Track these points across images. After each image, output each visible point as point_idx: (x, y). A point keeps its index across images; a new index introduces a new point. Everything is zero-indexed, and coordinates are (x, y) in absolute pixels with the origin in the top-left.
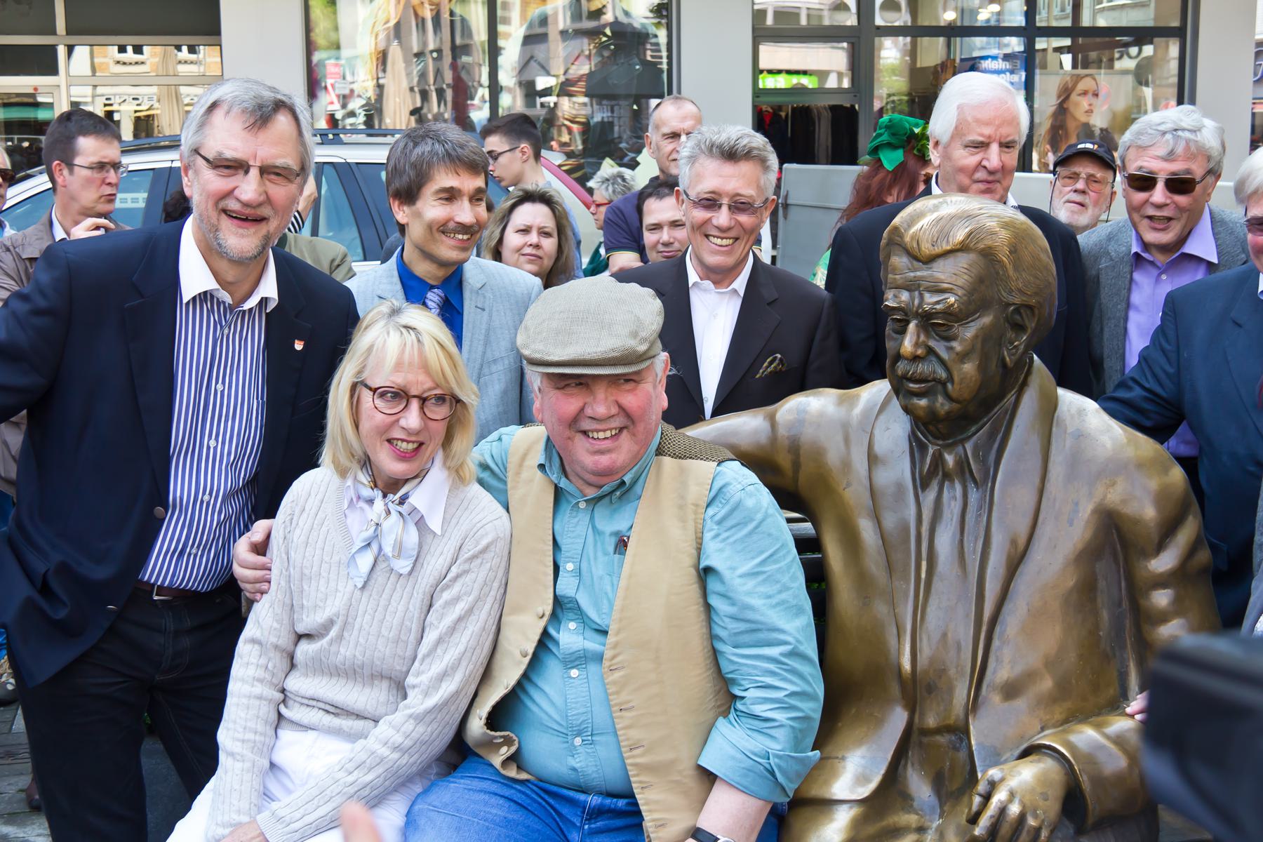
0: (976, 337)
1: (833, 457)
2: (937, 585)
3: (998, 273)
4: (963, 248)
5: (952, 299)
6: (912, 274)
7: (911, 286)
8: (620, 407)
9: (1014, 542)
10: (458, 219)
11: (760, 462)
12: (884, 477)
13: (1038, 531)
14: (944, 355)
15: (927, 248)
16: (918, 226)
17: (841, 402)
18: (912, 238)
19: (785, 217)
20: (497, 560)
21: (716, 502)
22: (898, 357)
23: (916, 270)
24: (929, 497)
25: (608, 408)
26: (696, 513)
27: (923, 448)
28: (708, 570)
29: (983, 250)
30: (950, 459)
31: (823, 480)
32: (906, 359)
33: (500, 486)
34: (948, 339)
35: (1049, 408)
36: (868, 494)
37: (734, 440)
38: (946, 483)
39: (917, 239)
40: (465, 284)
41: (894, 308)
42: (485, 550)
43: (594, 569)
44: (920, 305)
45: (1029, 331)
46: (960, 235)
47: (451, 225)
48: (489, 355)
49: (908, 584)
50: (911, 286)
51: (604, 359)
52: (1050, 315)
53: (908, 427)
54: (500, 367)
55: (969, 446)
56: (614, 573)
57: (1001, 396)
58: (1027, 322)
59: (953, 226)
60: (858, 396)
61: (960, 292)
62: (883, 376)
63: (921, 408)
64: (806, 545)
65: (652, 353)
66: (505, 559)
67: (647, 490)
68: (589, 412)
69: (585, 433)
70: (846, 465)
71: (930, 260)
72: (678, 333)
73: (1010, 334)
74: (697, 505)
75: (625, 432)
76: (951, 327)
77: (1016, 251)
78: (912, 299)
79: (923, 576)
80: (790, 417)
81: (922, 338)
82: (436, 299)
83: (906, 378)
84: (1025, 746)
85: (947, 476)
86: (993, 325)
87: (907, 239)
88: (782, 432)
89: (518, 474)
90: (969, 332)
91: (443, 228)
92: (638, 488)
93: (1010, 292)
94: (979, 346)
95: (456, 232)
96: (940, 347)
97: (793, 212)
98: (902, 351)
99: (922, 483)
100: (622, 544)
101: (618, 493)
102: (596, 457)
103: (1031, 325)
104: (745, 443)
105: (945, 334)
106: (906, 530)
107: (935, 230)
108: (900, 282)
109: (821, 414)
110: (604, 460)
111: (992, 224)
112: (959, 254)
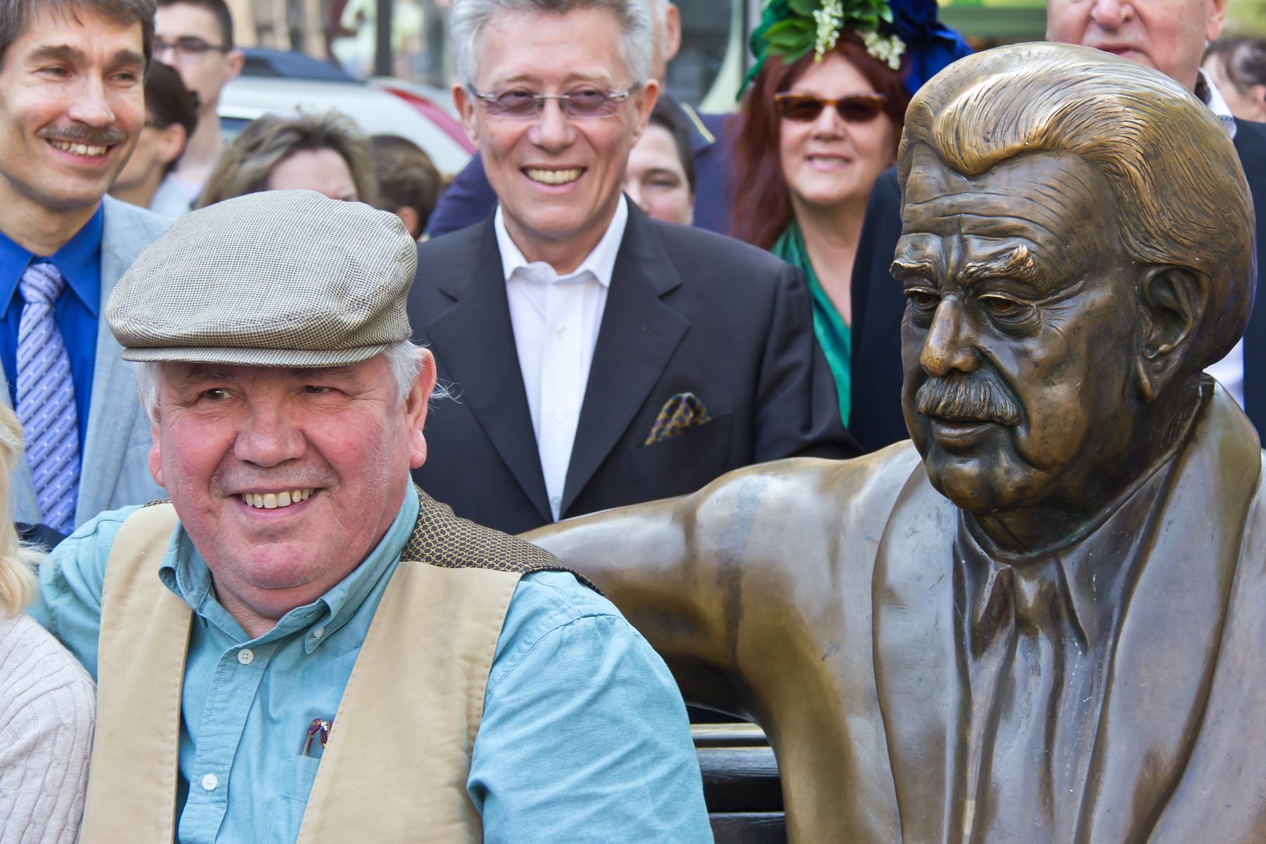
0: (1075, 330)
1: (807, 593)
3: (1119, 199)
4: (1047, 146)
5: (1022, 250)
6: (947, 201)
7: (945, 226)
8: (310, 443)
9: (1151, 759)
10: (77, 113)
11: (655, 608)
12: (896, 630)
13: (1206, 738)
14: (1011, 367)
15: (975, 147)
17: (825, 485)
18: (947, 126)
20: (56, 773)
21: (514, 653)
22: (922, 375)
24: (986, 671)
25: (283, 442)
26: (470, 676)
27: (978, 567)
28: (481, 792)
29: (1089, 150)
30: (1029, 590)
31: (787, 642)
32: (934, 375)
33: (87, 622)
37: (609, 561)
38: (1022, 639)
40: (106, 257)
41: (911, 272)
42: (28, 751)
43: (255, 786)
46: (1040, 119)
47: (63, 125)
50: (945, 226)
51: (269, 335)
52: (1239, 293)
55: (1070, 565)
56: (296, 794)
57: (1138, 462)
58: (1186, 306)
59: (1027, 102)
60: (862, 472)
61: (1040, 236)
65: (380, 333)
66: (76, 769)
67: (376, 632)
68: (242, 450)
69: (239, 497)
70: (834, 610)
71: (983, 170)
72: (465, 320)
73: (1151, 330)
74: (473, 660)
75: (322, 498)
76: (1023, 309)
77: (1157, 155)
78: (946, 250)
79: (968, 829)
80: (725, 513)
81: (966, 331)
82: (43, 283)
84: (195, 541)
85: (1024, 624)
86: (1109, 310)
87: (937, 128)
88: (707, 543)
89: (122, 596)
90: (1061, 319)
91: (48, 130)
92: (358, 623)
93: (1147, 238)
94: (1082, 348)
95: (73, 139)
96: (1002, 351)
99: (974, 639)
100: (316, 737)
101: (318, 632)
102: (261, 547)
103: (1195, 310)
104: (627, 563)
105: (1011, 323)
106: (937, 739)
107: (991, 109)
108: (923, 218)
109: (787, 507)
110: (276, 554)
111: (1109, 97)
112: (1040, 158)
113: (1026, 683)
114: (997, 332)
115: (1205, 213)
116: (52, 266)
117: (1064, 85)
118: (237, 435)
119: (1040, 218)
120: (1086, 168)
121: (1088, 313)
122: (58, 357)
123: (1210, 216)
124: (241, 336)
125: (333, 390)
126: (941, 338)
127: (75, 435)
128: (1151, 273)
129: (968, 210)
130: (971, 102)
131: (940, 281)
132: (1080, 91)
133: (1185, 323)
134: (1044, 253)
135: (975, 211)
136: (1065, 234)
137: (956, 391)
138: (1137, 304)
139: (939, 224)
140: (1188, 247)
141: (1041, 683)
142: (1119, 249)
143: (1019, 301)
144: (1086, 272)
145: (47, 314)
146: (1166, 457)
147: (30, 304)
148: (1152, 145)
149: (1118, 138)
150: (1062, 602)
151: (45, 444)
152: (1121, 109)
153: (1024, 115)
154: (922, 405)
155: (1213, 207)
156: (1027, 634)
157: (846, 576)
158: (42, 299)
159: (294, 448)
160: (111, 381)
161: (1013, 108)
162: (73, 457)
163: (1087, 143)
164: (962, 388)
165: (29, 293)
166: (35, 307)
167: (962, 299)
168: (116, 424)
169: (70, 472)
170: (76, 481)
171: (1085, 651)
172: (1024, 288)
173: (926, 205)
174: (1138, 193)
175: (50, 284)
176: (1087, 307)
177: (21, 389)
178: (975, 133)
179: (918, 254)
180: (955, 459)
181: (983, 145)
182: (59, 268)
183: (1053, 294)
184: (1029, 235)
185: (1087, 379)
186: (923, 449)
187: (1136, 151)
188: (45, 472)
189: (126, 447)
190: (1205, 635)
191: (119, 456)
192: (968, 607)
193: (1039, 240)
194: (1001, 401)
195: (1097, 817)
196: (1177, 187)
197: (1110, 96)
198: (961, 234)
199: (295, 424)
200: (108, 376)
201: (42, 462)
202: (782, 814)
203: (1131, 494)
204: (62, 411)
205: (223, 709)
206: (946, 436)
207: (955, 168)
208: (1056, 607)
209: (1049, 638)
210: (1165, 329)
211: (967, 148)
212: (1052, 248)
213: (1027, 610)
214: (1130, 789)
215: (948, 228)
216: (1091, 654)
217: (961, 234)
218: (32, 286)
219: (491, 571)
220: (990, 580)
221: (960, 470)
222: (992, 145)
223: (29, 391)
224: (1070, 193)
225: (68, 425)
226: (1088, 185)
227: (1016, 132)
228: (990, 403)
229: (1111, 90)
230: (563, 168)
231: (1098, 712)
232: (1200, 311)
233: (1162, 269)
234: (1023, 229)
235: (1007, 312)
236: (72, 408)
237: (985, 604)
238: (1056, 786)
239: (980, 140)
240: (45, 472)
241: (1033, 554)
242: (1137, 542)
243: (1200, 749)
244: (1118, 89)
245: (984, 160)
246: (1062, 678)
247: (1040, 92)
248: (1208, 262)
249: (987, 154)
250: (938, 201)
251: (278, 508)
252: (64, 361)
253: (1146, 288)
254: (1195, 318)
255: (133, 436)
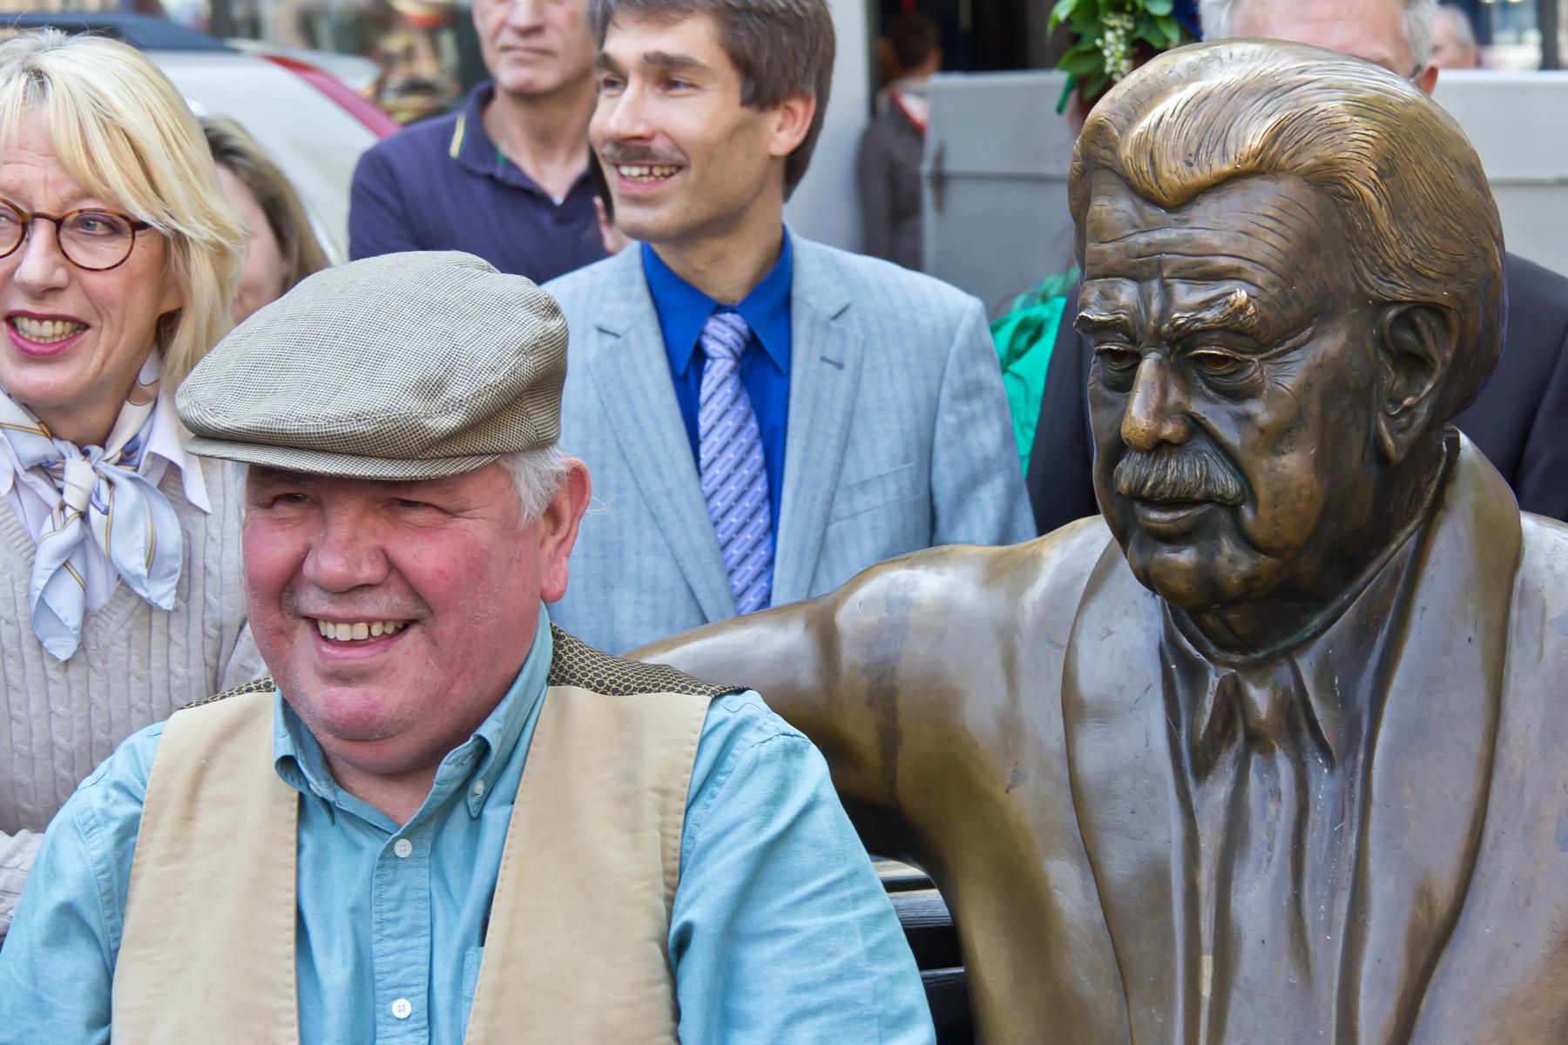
0: (1306, 386)
1: (979, 712)
2: (1240, 1011)
3: (1351, 227)
4: (1261, 167)
5: (1241, 295)
6: (1142, 239)
7: (1141, 269)
8: (392, 567)
9: (1424, 895)
13: (1485, 865)
14: (1231, 435)
15: (1174, 173)
16: (1150, 119)
18: (1138, 148)
19: (940, 205)
22: (1119, 448)
23: (1150, 228)
24: (1214, 795)
27: (1194, 674)
30: (1260, 698)
31: (956, 769)
32: (1139, 449)
34: (1238, 395)
35: (1503, 560)
36: (1065, 800)
38: (1255, 758)
39: (1147, 148)
41: (1101, 327)
44: (1165, 314)
45: (1439, 370)
46: (1253, 135)
48: (851, 474)
49: (1168, 1013)
50: (1141, 269)
51: (331, 437)
53: (1157, 625)
54: (875, 498)
55: (1306, 665)
57: (1380, 536)
61: (1260, 277)
62: (1092, 510)
63: (1181, 570)
64: (935, 945)
68: (309, 567)
69: (313, 621)
70: (1011, 727)
71: (1185, 200)
73: (1392, 380)
75: (413, 633)
76: (1242, 366)
78: (1145, 299)
79: (1206, 991)
80: (871, 618)
81: (1175, 395)
82: (728, 335)
83: (1142, 497)
85: (1256, 740)
87: (1126, 152)
90: (1289, 375)
93: (1385, 272)
94: (1314, 407)
96: (1218, 417)
97: (959, 195)
98: (1126, 430)
99: (1195, 760)
102: (334, 690)
103: (1442, 354)
105: (1228, 383)
106: (1157, 876)
107: (1192, 125)
108: (1112, 261)
109: (946, 608)
110: (349, 699)
111: (1331, 105)
112: (1255, 183)
113: (1264, 810)
114: (1211, 393)
115: (1451, 236)
116: (737, 317)
117: (1277, 93)
118: (307, 550)
119: (1258, 255)
120: (1309, 191)
121: (1320, 366)
122: (746, 420)
123: (1457, 241)
124: (298, 436)
125: (428, 505)
126: (1146, 404)
127: (766, 509)
128: (1392, 313)
129: (1170, 249)
130: (1166, 118)
131: (1139, 336)
132: (1297, 99)
133: (1433, 370)
134: (1265, 298)
135: (1180, 250)
136: (1288, 274)
137: (1166, 466)
138: (1375, 351)
139: (1133, 267)
140: (1435, 280)
141: (1283, 810)
142: (1352, 286)
143: (1238, 356)
144: (1315, 316)
145: (732, 371)
146: (1409, 529)
147: (713, 359)
148: (1387, 160)
149: (1347, 154)
150: (1300, 710)
151: (734, 519)
152: (1348, 118)
153: (1233, 132)
154: (1123, 485)
155: (1460, 229)
156: (1261, 752)
157: (1026, 689)
158: (727, 353)
159: (369, 571)
160: (807, 449)
161: (1219, 124)
162: (765, 534)
163: (1311, 162)
164: (1173, 463)
165: (711, 347)
166: (719, 363)
167: (1167, 356)
168: (814, 498)
169: (763, 552)
170: (771, 562)
171: (1332, 768)
172: (1243, 340)
173: (1115, 244)
174: (1373, 218)
175: (736, 337)
176: (1319, 358)
177: (705, 457)
178: (1175, 155)
179: (1109, 304)
180: (1166, 548)
181: (1185, 170)
182: (746, 319)
183: (1277, 346)
184: (1248, 276)
185: (1321, 445)
186: (1122, 535)
187: (1369, 169)
188: (735, 552)
189: (826, 523)
190: (1475, 741)
191: (819, 534)
192: (1184, 721)
193: (1259, 282)
194: (1221, 477)
195: (1367, 968)
196: (1417, 209)
197: (1334, 104)
198: (1162, 279)
199: (374, 542)
200: (803, 442)
201: (731, 540)
202: (961, 970)
203: (1374, 576)
204: (752, 482)
205: (397, 920)
206: (1156, 521)
207: (1150, 199)
208: (1294, 713)
209: (1287, 755)
210: (1408, 378)
211: (1166, 174)
212: (1274, 291)
213: (1261, 723)
214: (1402, 933)
215: (1146, 271)
216: (1339, 771)
217: (1162, 279)
218: (715, 339)
219: (672, 694)
220: (1210, 689)
221: (1173, 561)
222: (1196, 169)
223: (714, 460)
224: (1293, 223)
225: (759, 497)
226: (1314, 212)
227: (1224, 153)
228: (1208, 480)
229: (1334, 96)
230: (54, 318)
231: (1353, 841)
232: (1449, 355)
233: (1403, 307)
234: (1239, 270)
235: (1223, 369)
236: (763, 478)
237: (1206, 719)
238: (1309, 933)
239: (1181, 164)
240: (735, 552)
241: (1261, 655)
242: (1383, 634)
243: (1478, 878)
244: (1342, 94)
245: (1187, 188)
246: (1307, 803)
247: (1250, 102)
248: (1457, 297)
249: (1191, 181)
250: (1132, 239)
251: (353, 641)
252: (753, 425)
253: (1386, 332)
254: (1444, 363)
255: (835, 510)
